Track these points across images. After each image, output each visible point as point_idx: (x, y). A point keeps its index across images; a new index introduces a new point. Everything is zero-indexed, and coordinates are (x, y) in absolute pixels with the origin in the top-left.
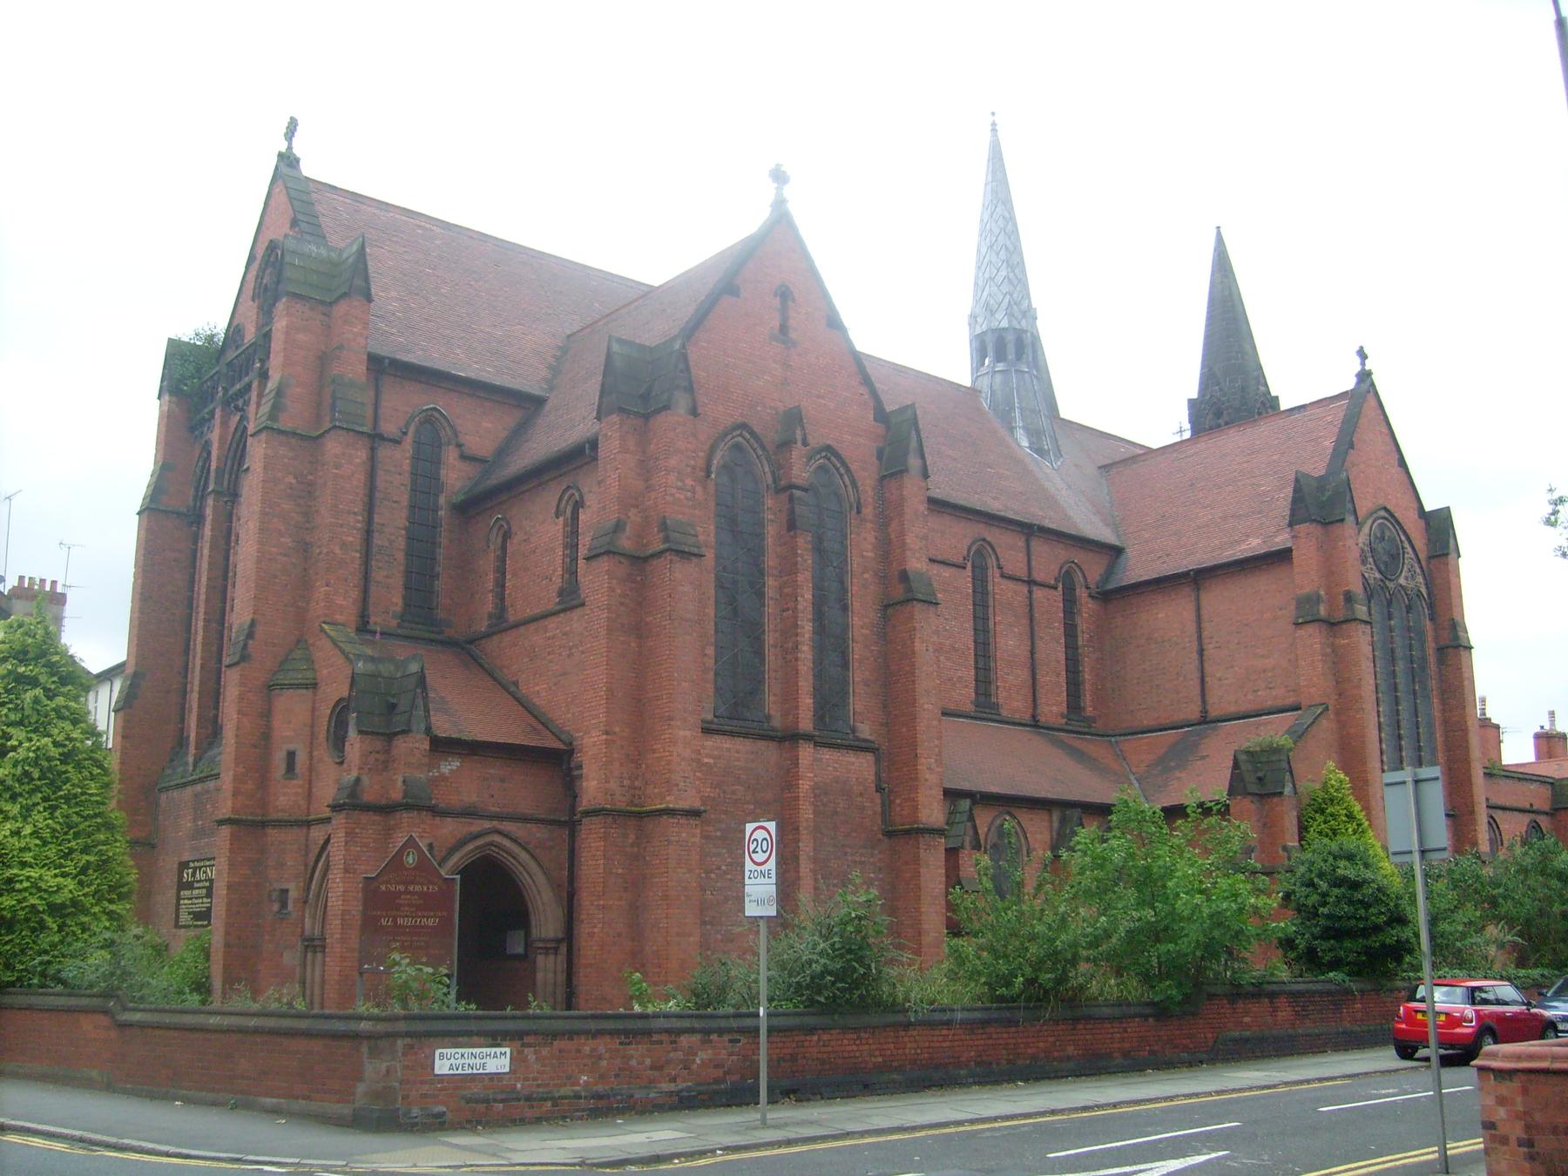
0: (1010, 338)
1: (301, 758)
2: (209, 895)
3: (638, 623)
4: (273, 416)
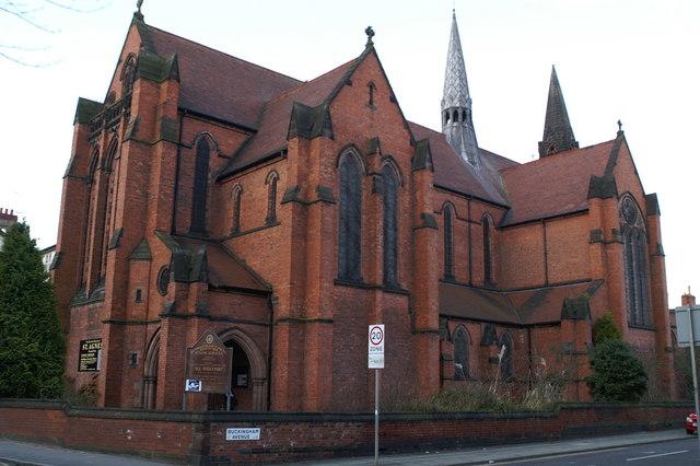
0: (460, 112)
1: (144, 293)
2: (96, 356)
3: (301, 234)
4: (133, 133)
